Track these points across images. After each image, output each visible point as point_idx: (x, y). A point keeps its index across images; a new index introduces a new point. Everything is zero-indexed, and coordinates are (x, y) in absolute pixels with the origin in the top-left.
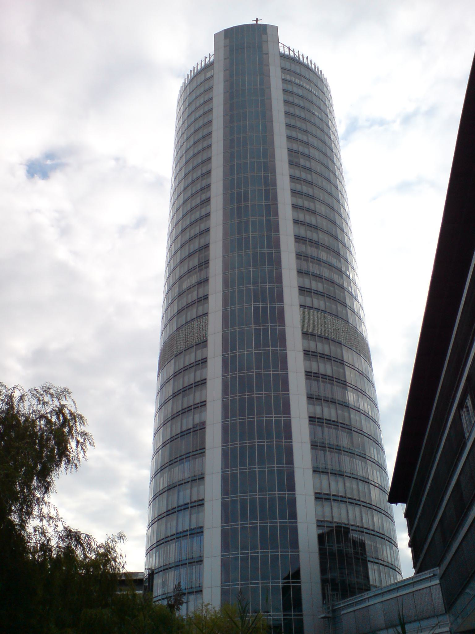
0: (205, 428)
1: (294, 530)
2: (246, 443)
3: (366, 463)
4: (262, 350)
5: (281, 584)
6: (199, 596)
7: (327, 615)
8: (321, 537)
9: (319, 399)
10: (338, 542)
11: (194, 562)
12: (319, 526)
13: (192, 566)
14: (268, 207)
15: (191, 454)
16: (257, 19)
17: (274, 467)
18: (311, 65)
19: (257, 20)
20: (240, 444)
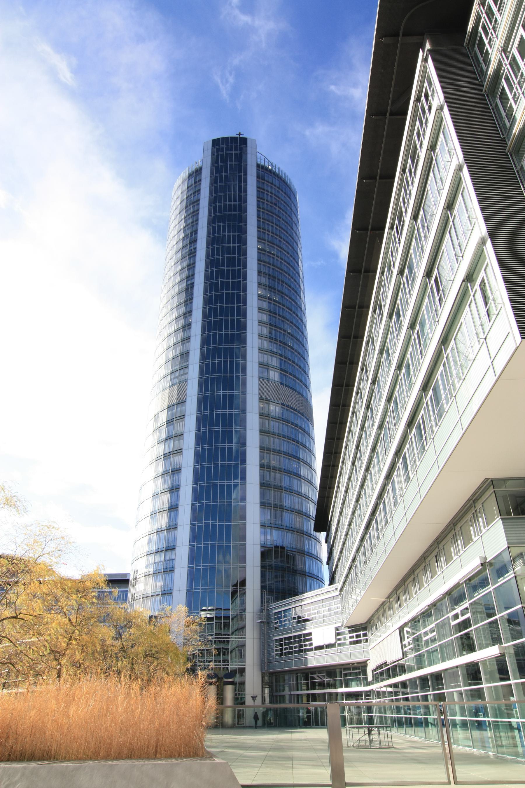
0: (178, 508)
1: (244, 549)
2: (212, 446)
3: (304, 557)
4: (227, 428)
5: (231, 590)
6: (173, 552)
7: (263, 621)
8: (263, 554)
9: (268, 432)
10: (276, 558)
11: (166, 594)
12: (261, 547)
13: (166, 574)
14: (240, 187)
15: (175, 419)
16: (240, 133)
17: (232, 464)
18: (282, 175)
19: (240, 134)
20: (209, 412)
